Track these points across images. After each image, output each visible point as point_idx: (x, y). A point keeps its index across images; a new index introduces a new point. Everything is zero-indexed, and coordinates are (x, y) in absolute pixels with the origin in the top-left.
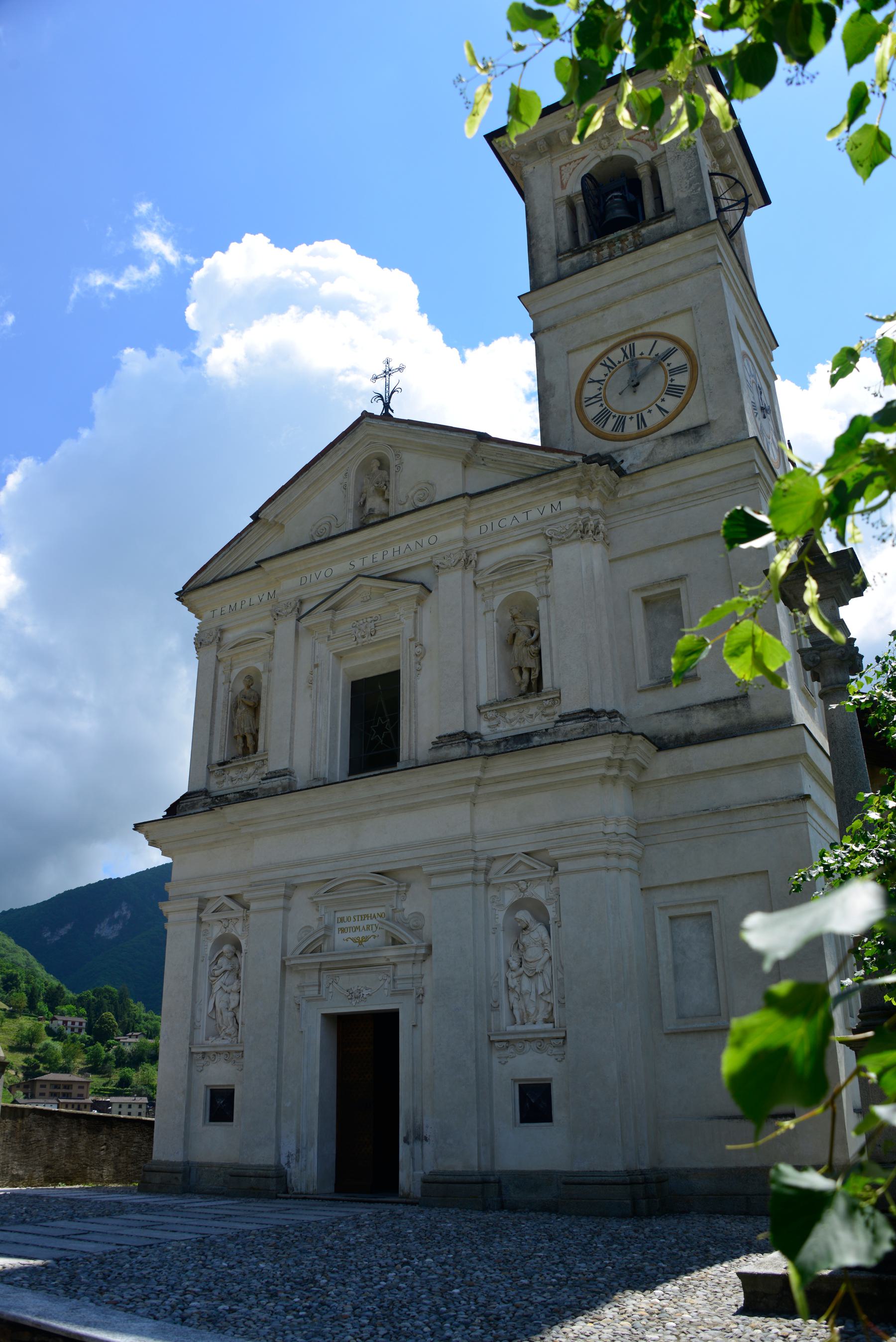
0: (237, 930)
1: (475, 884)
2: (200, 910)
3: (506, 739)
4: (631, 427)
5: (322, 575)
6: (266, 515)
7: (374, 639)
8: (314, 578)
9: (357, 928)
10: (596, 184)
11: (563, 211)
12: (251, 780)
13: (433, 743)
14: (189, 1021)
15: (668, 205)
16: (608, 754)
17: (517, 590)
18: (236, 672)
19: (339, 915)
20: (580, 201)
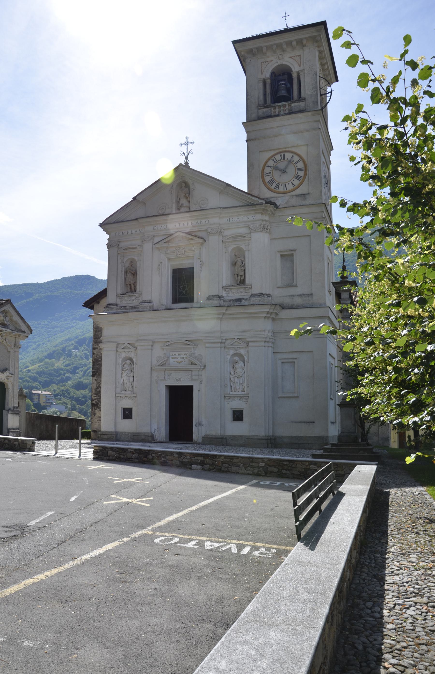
0: (132, 355)
1: (221, 347)
2: (117, 347)
3: (233, 300)
4: (281, 189)
5: (163, 227)
7: (183, 256)
8: (159, 228)
10: (275, 76)
11: (261, 85)
12: (134, 302)
13: (207, 298)
14: (114, 385)
15: (303, 95)
16: (268, 310)
18: (125, 259)
19: (171, 353)
20: (268, 82)
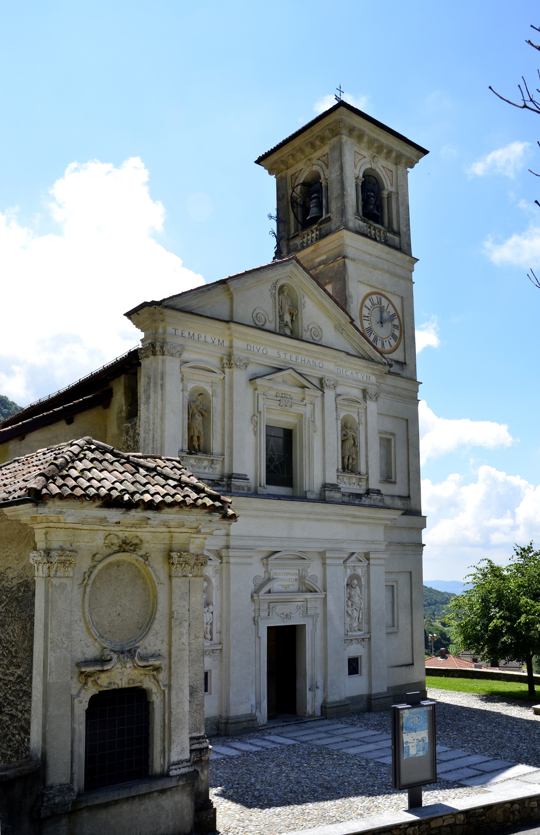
6: (231, 285)
9: (284, 580)
17: (350, 413)
